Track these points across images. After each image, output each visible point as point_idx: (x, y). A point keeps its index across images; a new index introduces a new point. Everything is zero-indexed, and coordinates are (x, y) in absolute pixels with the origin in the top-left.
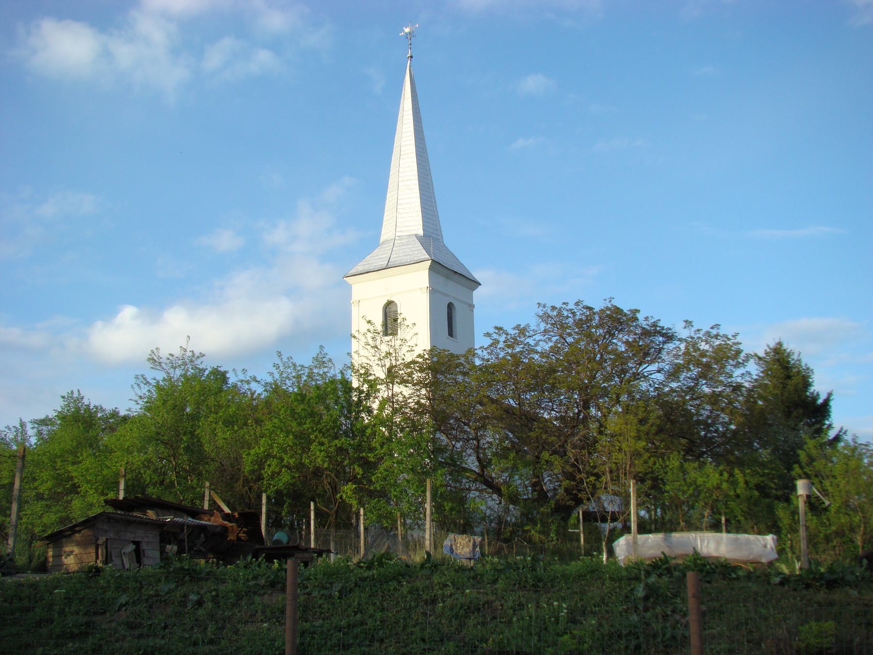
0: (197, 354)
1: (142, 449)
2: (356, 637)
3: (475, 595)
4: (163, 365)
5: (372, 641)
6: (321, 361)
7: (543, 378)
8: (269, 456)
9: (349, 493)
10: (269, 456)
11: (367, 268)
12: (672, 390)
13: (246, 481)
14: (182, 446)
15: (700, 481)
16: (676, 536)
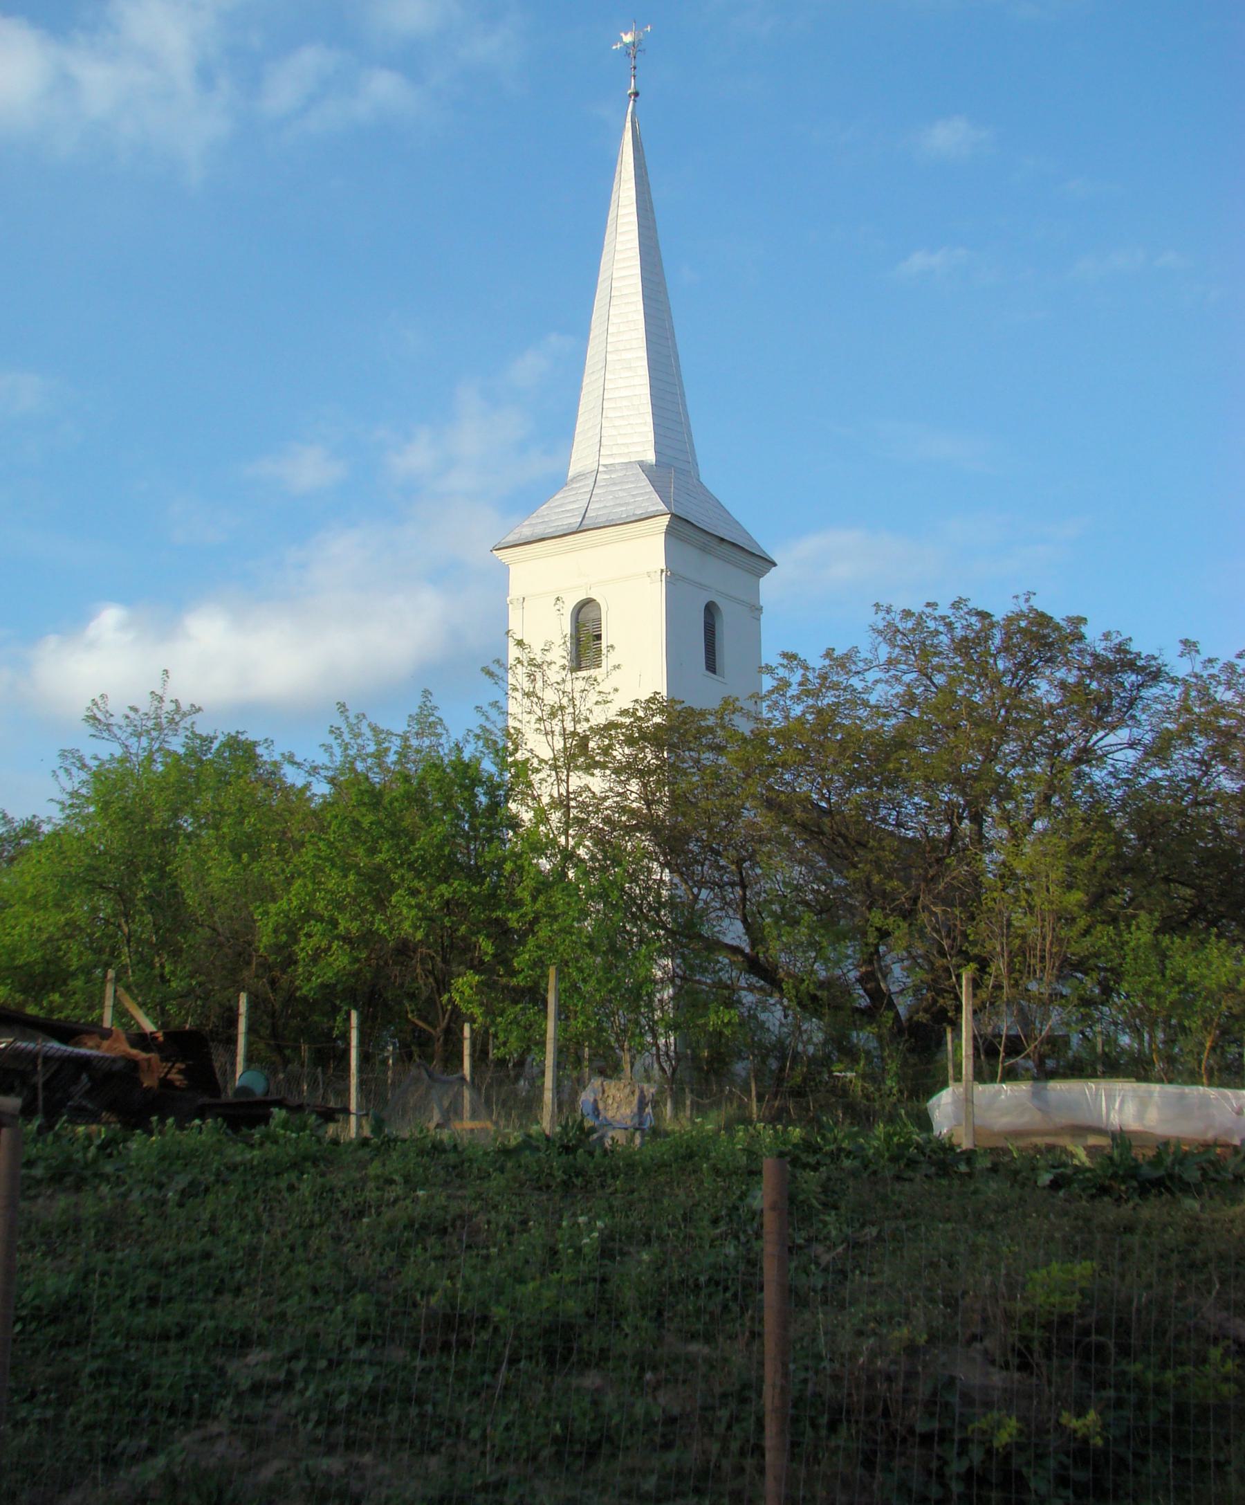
0: (185, 707)
1: (61, 903)
3: (441, 1200)
4: (115, 729)
5: (218, 1292)
6: (427, 722)
8: (309, 916)
10: (309, 916)
11: (540, 531)
12: (1154, 785)
13: (265, 966)
14: (141, 895)
15: (1192, 974)
16: (1058, 1088)
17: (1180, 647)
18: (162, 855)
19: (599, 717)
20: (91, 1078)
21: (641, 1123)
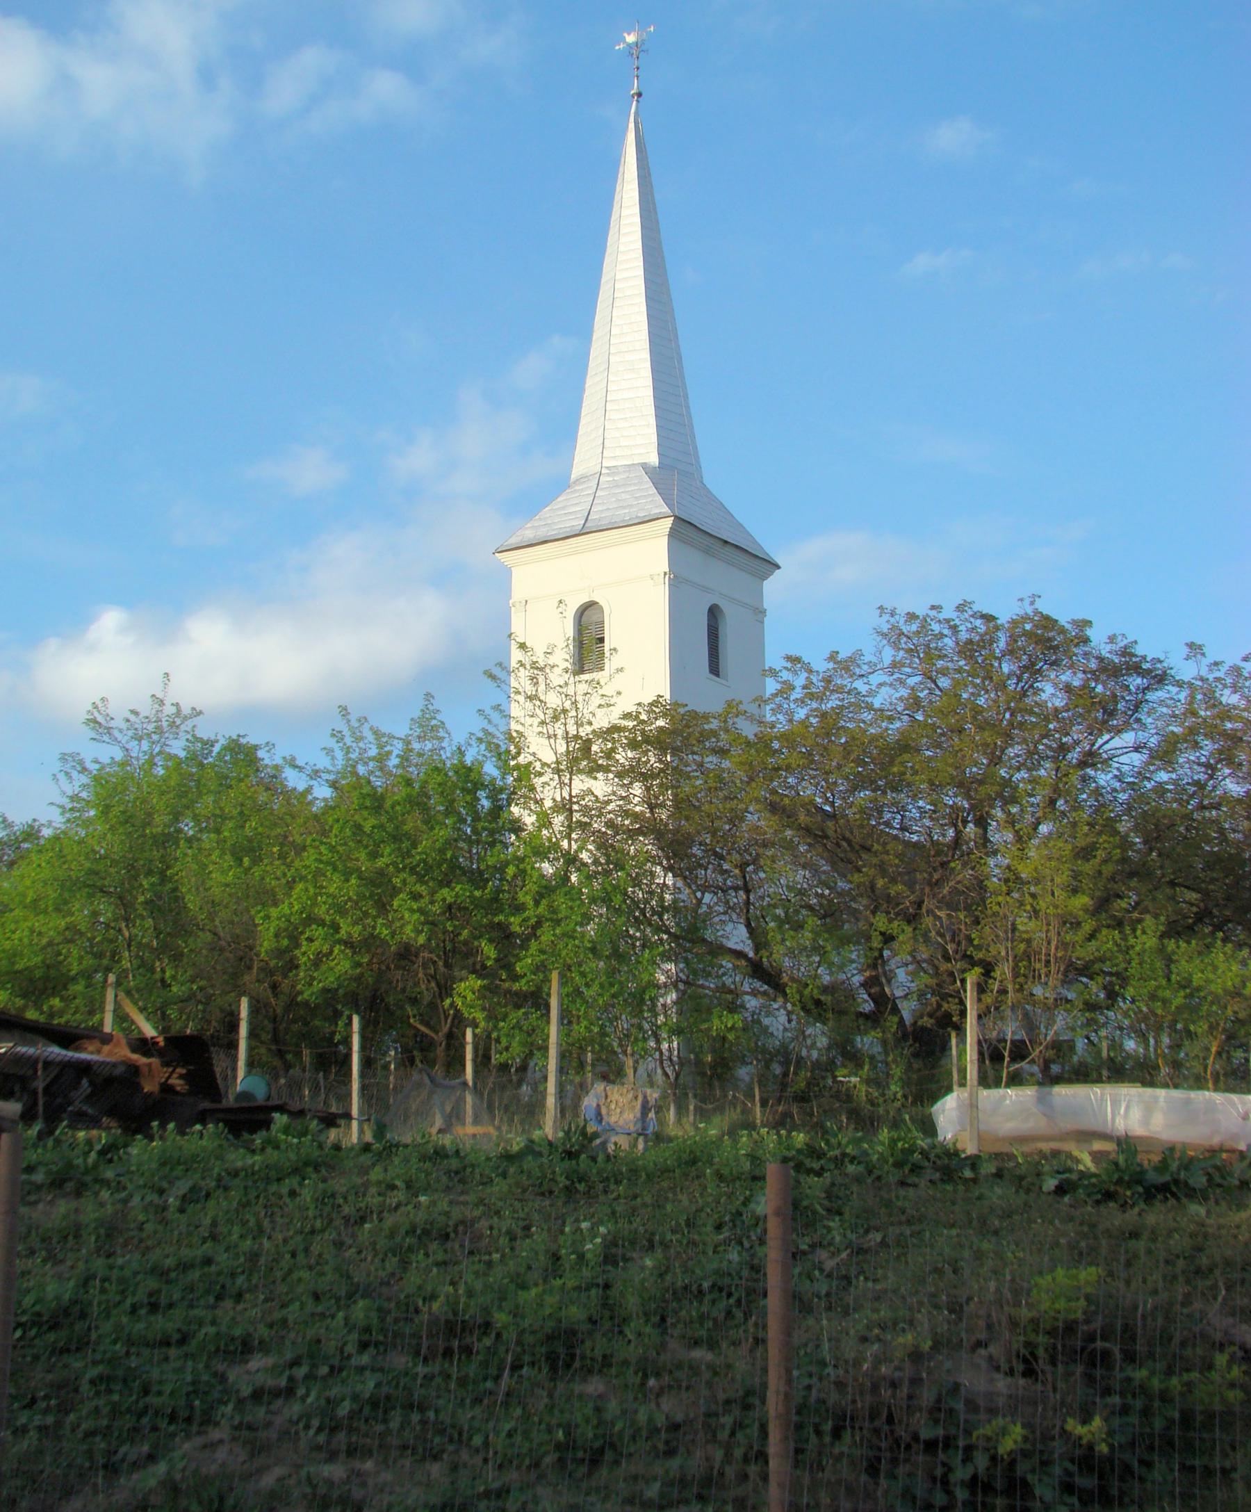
0: (186, 710)
1: (61, 907)
2: (191, 1288)
3: (443, 1205)
6: (429, 725)
7: (885, 764)
8: (310, 920)
9: (470, 996)
10: (310, 920)
11: (543, 533)
12: (1160, 789)
13: (267, 971)
14: (141, 899)
16: (1063, 1093)
17: (1186, 650)
18: (163, 859)
19: (602, 721)
20: (91, 1083)
21: (644, 1128)
